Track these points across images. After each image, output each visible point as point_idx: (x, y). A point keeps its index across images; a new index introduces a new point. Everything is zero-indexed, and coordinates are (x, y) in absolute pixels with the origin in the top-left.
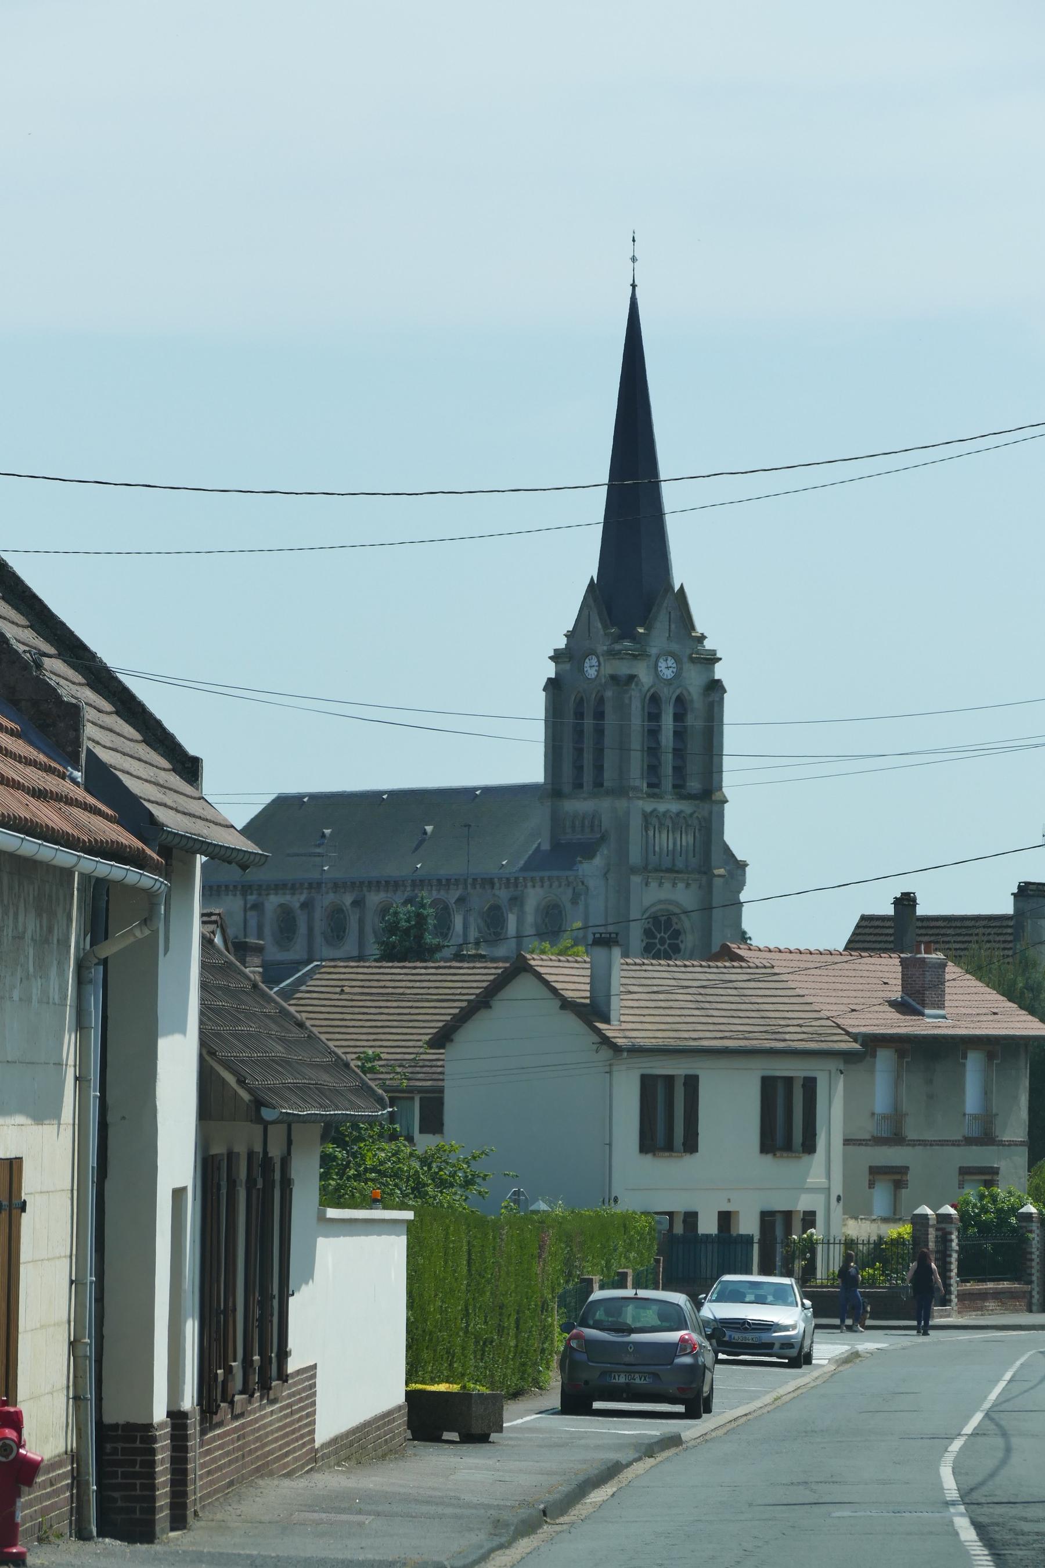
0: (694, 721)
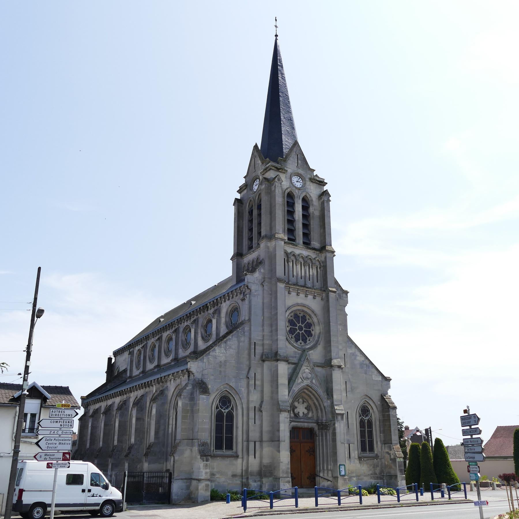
0: (315, 210)
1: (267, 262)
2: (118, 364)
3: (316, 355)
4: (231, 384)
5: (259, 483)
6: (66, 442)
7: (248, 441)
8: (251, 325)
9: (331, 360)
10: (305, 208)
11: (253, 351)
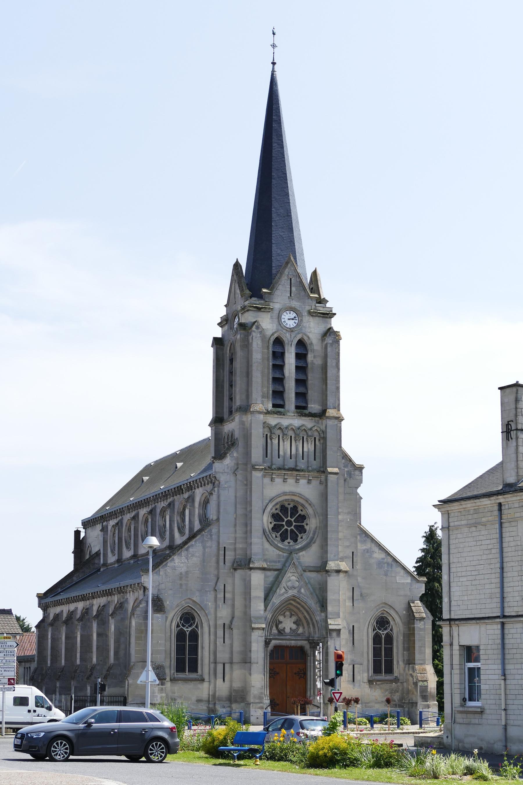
1: (241, 443)
2: (89, 541)
3: (308, 557)
4: (194, 599)
5: (229, 709)
6: (10, 669)
7: (215, 663)
8: (219, 526)
9: (325, 563)
10: (301, 356)
11: (222, 558)
